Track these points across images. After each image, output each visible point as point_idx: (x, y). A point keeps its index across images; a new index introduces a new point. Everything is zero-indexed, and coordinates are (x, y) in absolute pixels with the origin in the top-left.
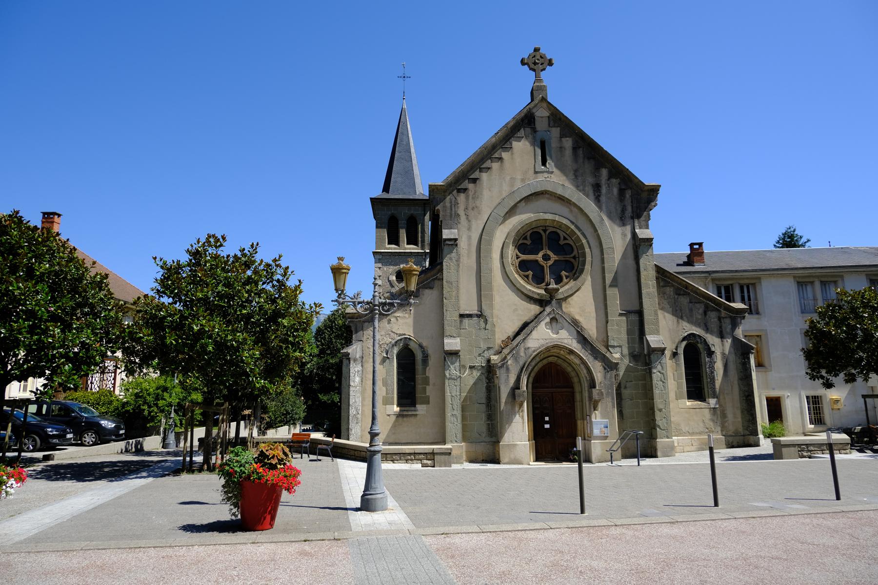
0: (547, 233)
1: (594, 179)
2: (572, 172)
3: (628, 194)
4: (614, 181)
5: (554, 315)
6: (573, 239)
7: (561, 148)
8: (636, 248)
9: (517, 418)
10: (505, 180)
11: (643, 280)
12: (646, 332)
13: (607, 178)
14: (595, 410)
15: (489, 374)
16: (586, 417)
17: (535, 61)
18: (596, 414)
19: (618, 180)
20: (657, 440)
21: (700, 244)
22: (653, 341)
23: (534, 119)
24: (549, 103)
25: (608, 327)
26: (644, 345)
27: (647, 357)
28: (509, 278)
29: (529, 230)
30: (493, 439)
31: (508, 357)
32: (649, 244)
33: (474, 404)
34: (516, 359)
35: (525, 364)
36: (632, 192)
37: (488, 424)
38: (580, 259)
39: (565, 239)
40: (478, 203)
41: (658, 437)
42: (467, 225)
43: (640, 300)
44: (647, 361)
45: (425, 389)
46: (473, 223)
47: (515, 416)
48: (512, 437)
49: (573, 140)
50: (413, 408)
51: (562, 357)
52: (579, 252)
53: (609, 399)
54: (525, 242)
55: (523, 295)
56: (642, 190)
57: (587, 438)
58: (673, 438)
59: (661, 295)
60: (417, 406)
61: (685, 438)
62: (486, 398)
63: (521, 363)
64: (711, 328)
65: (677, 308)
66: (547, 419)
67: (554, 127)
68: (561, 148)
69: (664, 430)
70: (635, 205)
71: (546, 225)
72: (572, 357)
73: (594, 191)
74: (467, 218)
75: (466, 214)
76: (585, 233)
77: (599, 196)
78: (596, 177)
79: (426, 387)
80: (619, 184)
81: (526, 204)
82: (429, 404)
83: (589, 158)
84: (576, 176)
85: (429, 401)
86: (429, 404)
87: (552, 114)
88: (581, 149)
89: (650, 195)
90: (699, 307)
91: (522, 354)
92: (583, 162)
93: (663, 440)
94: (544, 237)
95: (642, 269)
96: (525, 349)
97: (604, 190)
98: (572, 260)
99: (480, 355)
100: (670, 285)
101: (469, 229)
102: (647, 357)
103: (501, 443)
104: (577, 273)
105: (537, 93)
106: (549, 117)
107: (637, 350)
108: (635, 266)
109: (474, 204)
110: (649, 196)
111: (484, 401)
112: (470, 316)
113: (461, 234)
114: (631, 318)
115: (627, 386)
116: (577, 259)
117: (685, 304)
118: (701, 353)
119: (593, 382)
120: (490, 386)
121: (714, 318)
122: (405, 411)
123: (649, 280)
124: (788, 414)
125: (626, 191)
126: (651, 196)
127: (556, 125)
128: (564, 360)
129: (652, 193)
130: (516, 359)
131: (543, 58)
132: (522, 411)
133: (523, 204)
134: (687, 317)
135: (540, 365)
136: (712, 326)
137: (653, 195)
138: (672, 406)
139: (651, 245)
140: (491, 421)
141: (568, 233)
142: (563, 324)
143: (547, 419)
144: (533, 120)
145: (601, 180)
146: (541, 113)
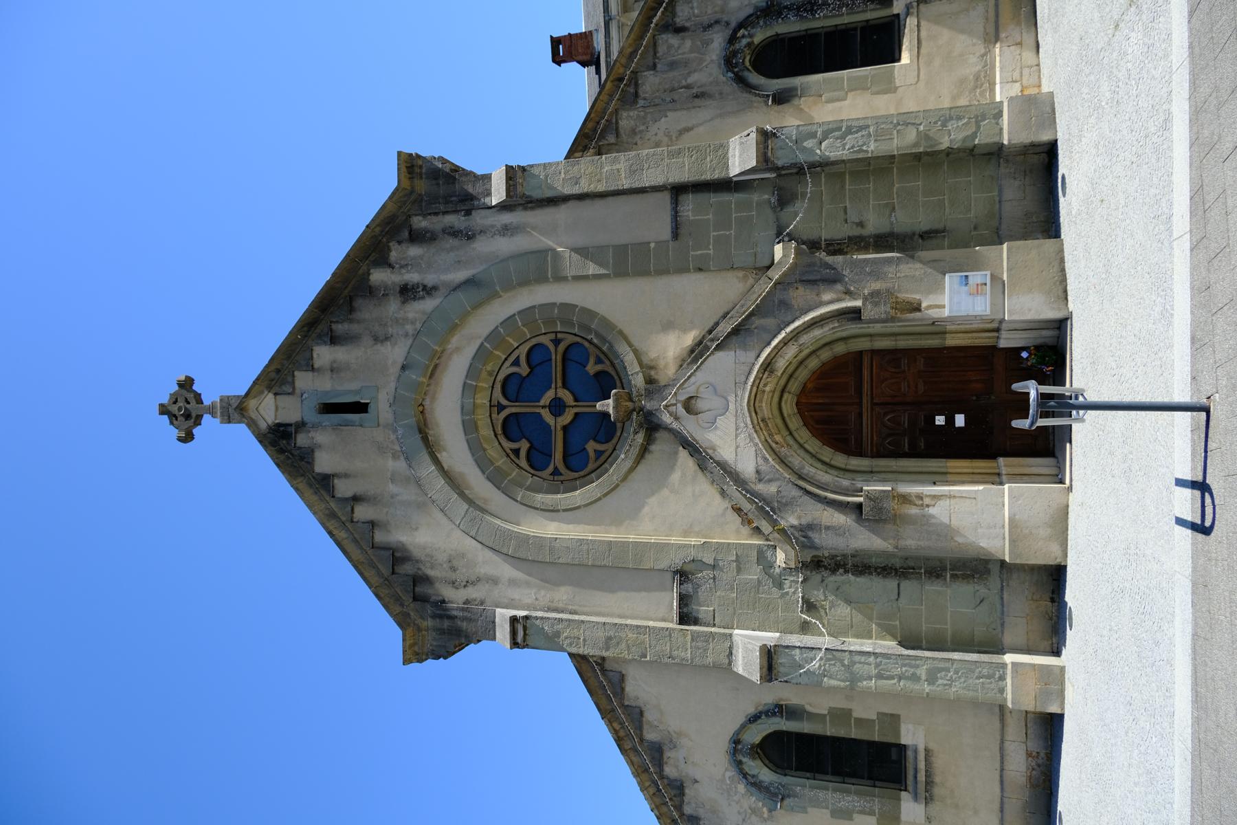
0: (504, 402)
1: (392, 298)
2: (379, 346)
3: (420, 222)
4: (394, 255)
5: (679, 405)
6: (516, 345)
7: (332, 371)
8: (531, 202)
9: (939, 512)
10: (397, 495)
11: (601, 188)
12: (723, 175)
13: (389, 270)
14: (917, 308)
15: (824, 566)
16: (937, 328)
17: (181, 415)
18: (929, 307)
19: (393, 245)
20: (1006, 142)
21: (555, 42)
22: (742, 162)
23: (279, 425)
24: (247, 394)
25: (539, 560)
26: (754, 180)
27: (783, 172)
28: (599, 499)
29: (500, 444)
30: (995, 569)
31: (783, 523)
32: (519, 174)
33: (899, 608)
34: (786, 504)
35: (801, 488)
36: (416, 215)
37: (954, 577)
38: (559, 329)
39: (516, 363)
40: (442, 558)
41: (996, 139)
42: (487, 586)
43: (647, 192)
44: (794, 171)
45: (860, 721)
46: (482, 571)
47: (933, 516)
48: (989, 527)
49: (318, 344)
50: (910, 753)
51: (783, 382)
52: (543, 332)
53: (890, 270)
54: (523, 453)
55: (639, 467)
56: (412, 192)
57: (995, 325)
58: (998, 99)
59: (637, 138)
60: (903, 742)
61: (998, 64)
62: (884, 577)
63: (795, 492)
64: (716, 12)
65: (668, 99)
66: (940, 420)
67: (293, 382)
68: (334, 369)
69: (978, 127)
70: (442, 208)
71: (488, 405)
72: (781, 364)
73: (415, 299)
74: (473, 583)
75: (465, 586)
76: (501, 321)
77: (425, 287)
78: (387, 295)
79: (855, 718)
80: (399, 243)
81: (444, 450)
82: (898, 716)
83: (352, 310)
84: (387, 339)
85: (892, 715)
86: (898, 716)
87: (269, 388)
88: (334, 326)
89: (421, 174)
90: (665, 48)
91: (772, 489)
92: (358, 322)
93: (1005, 127)
94: (514, 410)
95: (576, 190)
96: (760, 480)
97: (413, 277)
98: (562, 347)
99: (780, 586)
100: (614, 121)
101: (494, 581)
102: (783, 172)
103: (1007, 559)
104: (589, 337)
105: (234, 410)
106: (276, 394)
107: (766, 196)
108: (571, 204)
109: (445, 566)
110: (424, 176)
111: (892, 584)
112: (684, 600)
113: (506, 601)
114: (690, 213)
115: (857, 221)
116: (559, 336)
117: (657, 80)
118: (777, 35)
119: (844, 314)
120: (855, 566)
121: (692, 8)
122: (916, 777)
123: (601, 173)
124: (974, 460)
125: (415, 227)
126: (424, 171)
127: (290, 379)
128: (791, 376)
129: (417, 170)
130: (786, 504)
131: (177, 399)
132: (920, 497)
133: (443, 457)
134: (689, 74)
135: (804, 434)
136: (709, 12)
137: (421, 167)
138: (911, 106)
139: (523, 169)
140: (944, 569)
141: (504, 357)
142: (698, 384)
143: (940, 420)
144: (282, 429)
145: (393, 283)
146: (269, 410)
